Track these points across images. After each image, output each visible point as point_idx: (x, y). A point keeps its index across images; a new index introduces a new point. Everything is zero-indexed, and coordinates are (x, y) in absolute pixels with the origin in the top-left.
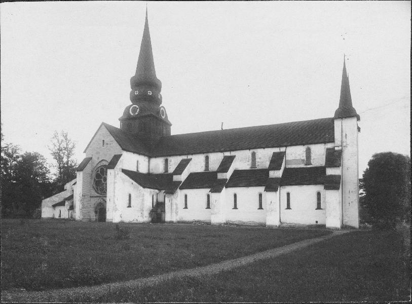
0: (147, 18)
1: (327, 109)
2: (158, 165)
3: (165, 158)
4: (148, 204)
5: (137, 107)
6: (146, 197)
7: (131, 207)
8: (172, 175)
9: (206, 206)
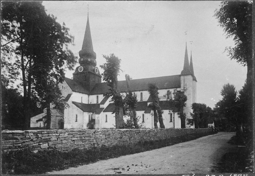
0: (88, 17)
1: (176, 69)
2: (93, 99)
3: (97, 95)
4: (87, 120)
5: (82, 67)
6: (86, 117)
7: (144, 122)
8: (99, 105)
9: (170, 121)
